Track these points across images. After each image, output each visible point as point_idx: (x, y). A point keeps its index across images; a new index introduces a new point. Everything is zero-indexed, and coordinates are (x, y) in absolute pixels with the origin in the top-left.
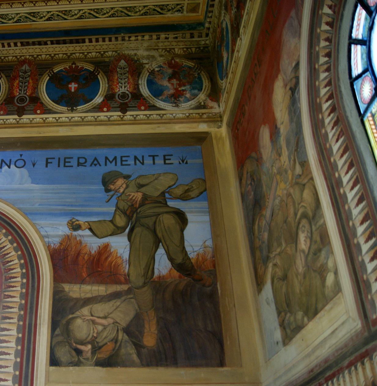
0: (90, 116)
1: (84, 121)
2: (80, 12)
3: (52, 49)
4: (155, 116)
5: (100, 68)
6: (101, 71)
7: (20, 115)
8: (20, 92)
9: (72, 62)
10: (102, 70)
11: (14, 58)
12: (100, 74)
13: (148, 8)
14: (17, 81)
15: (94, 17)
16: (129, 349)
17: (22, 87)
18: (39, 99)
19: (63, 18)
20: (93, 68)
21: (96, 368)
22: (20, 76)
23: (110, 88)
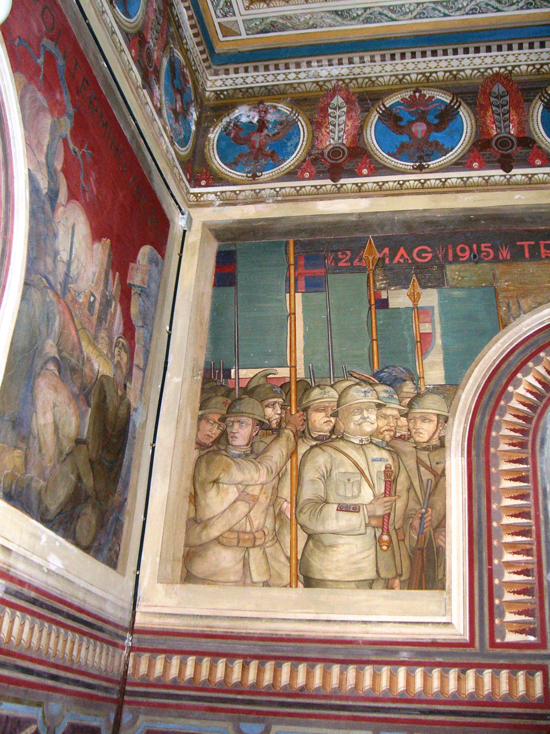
0: (454, 177)
1: (532, 182)
2: (365, 11)
3: (424, 65)
4: (412, 182)
5: (461, 97)
6: (462, 102)
7: (507, 168)
8: (498, 131)
9: (414, 89)
10: (464, 100)
11: (420, 76)
12: (461, 108)
13: (371, 11)
14: (490, 113)
15: (495, 10)
16: (340, 557)
17: (334, 133)
18: (534, 142)
19: (391, 18)
20: (450, 98)
21: (264, 588)
22: (491, 104)
23: (480, 128)
